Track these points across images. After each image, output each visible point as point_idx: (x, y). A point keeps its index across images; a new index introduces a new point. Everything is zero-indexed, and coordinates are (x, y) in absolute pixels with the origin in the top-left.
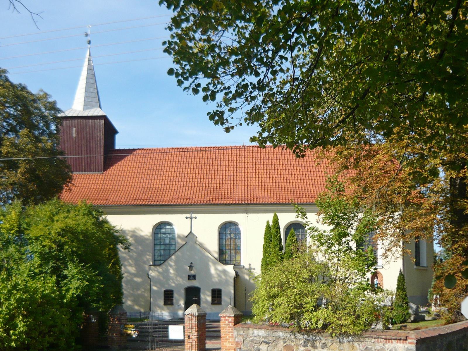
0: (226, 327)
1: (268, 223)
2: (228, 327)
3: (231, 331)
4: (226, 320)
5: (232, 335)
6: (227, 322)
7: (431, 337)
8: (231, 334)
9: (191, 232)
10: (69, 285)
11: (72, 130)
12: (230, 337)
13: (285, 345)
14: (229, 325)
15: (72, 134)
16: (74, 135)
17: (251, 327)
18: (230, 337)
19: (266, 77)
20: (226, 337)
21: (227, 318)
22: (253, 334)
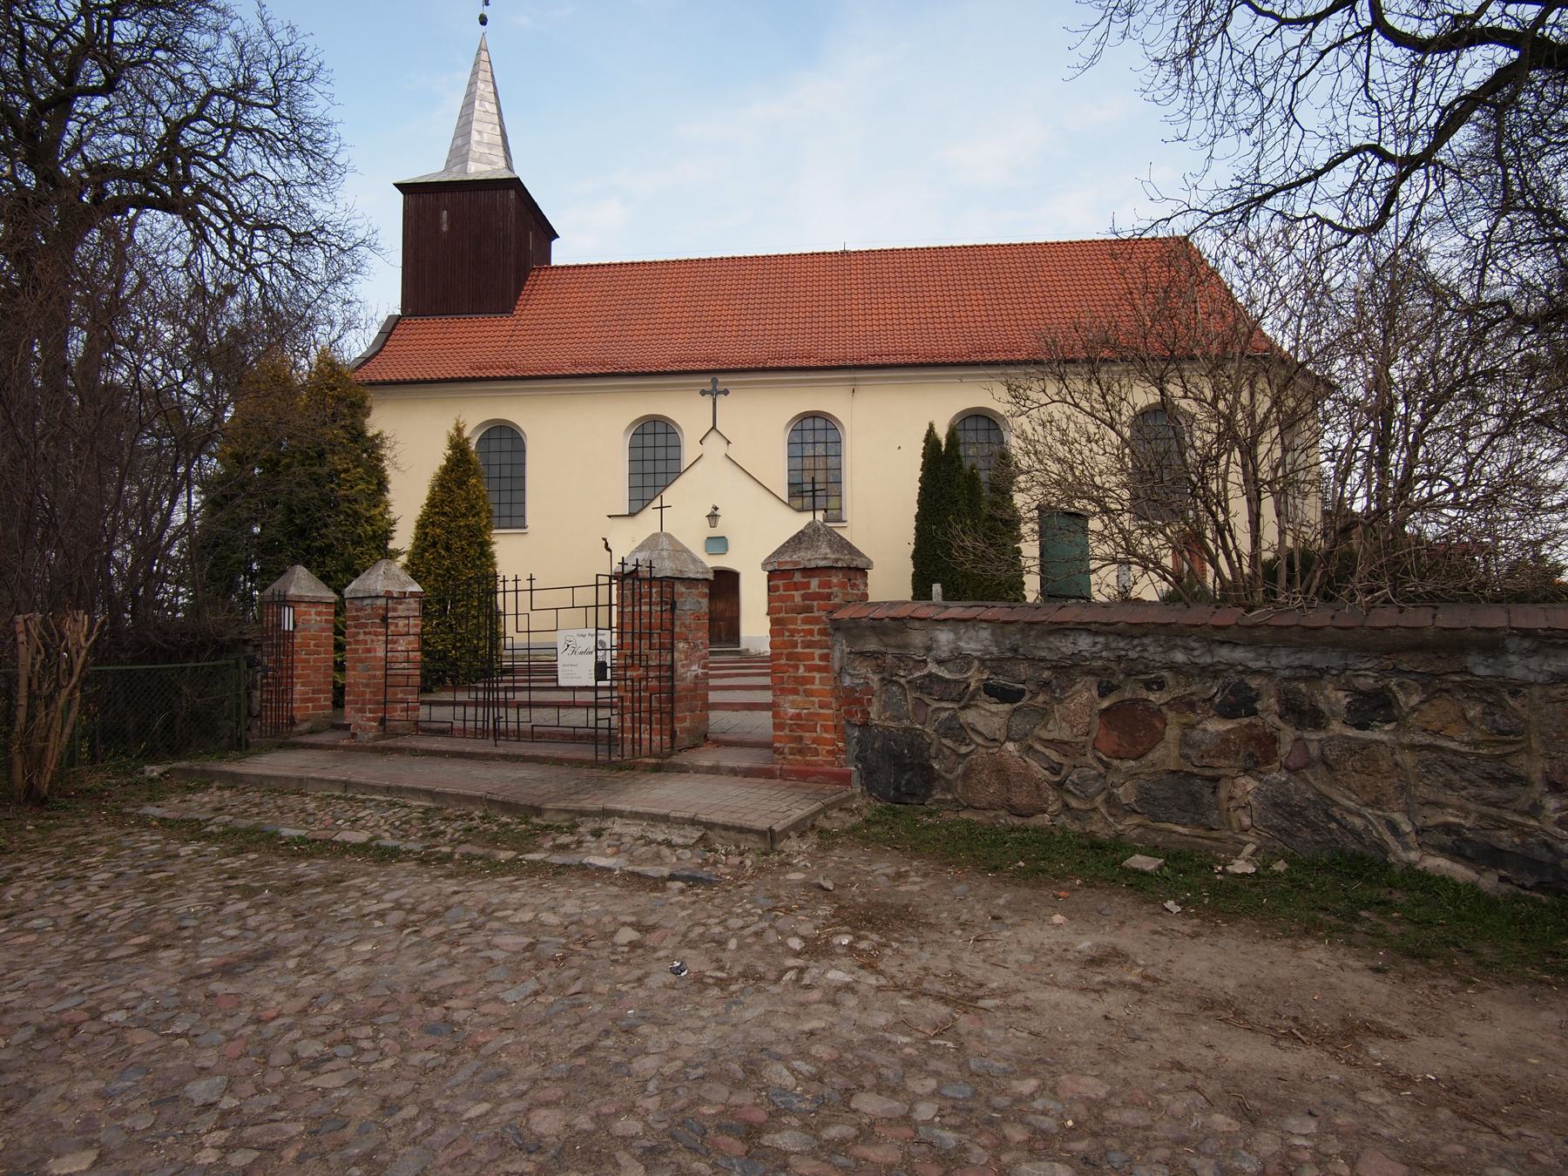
0: (794, 621)
1: (931, 433)
2: (805, 621)
3: (817, 638)
4: (796, 587)
5: (824, 657)
6: (797, 595)
7: (921, 502)
8: (818, 652)
9: (714, 427)
10: (1276, 430)
11: (438, 216)
12: (810, 669)
13: (1105, 704)
14: (809, 609)
15: (438, 225)
16: (445, 228)
17: (1248, 881)
18: (810, 669)
19: (1313, 183)
20: (797, 668)
21: (798, 578)
22: (929, 649)
